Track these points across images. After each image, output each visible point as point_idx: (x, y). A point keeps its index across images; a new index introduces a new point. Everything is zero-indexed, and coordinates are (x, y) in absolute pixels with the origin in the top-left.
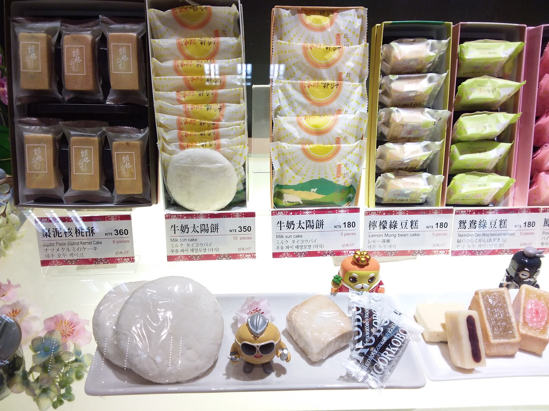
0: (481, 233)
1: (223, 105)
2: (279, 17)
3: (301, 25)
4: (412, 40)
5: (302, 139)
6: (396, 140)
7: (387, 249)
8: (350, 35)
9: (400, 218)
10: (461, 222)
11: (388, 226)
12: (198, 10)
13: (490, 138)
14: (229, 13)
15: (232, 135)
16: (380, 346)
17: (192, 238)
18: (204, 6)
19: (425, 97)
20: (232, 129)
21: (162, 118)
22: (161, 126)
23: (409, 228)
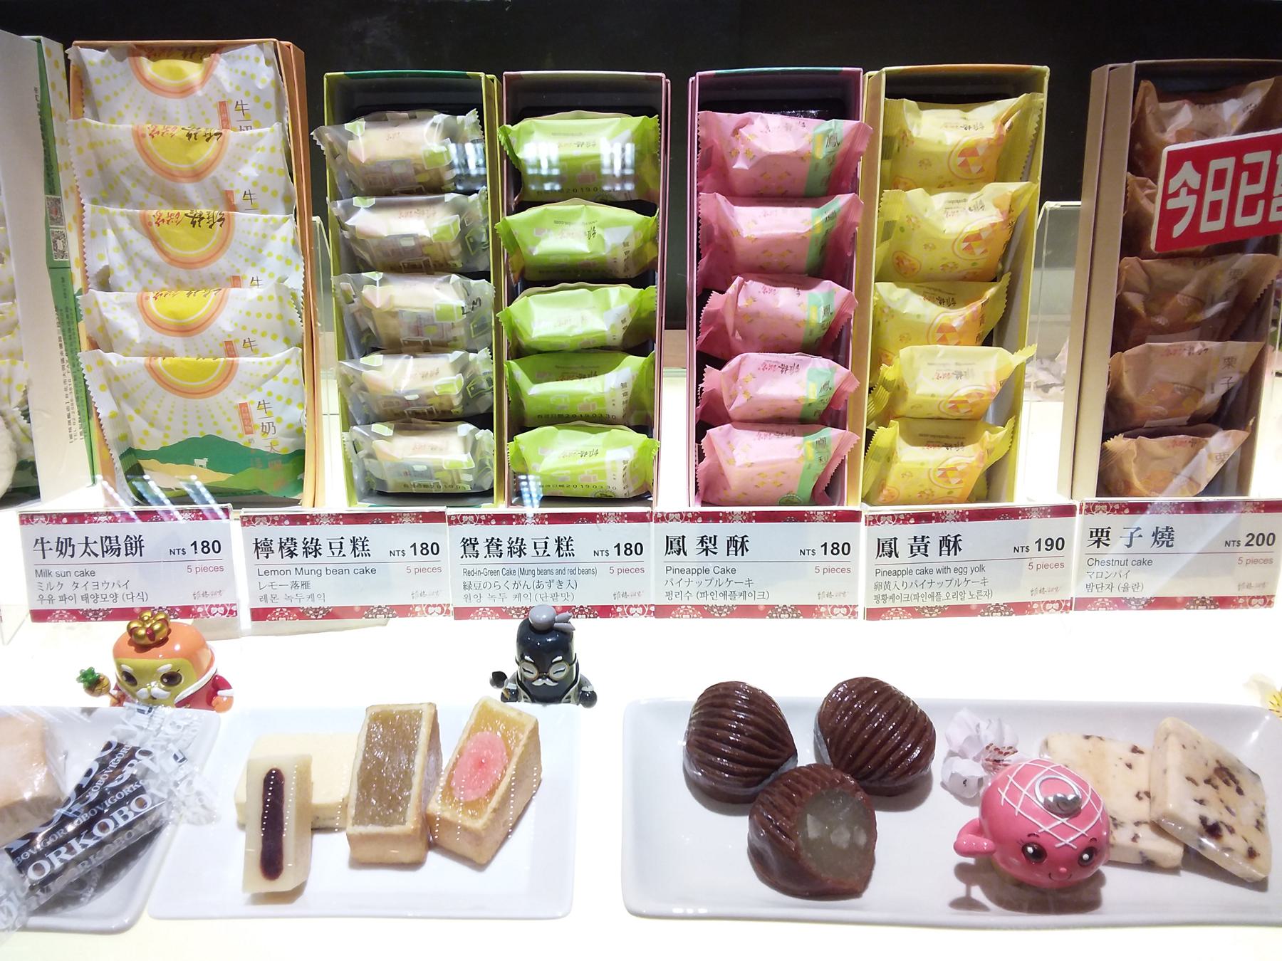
0: (516, 568)
4: (405, 114)
5: (147, 344)
6: (394, 347)
7: (305, 604)
8: (249, 104)
11: (300, 550)
17: (82, 568)
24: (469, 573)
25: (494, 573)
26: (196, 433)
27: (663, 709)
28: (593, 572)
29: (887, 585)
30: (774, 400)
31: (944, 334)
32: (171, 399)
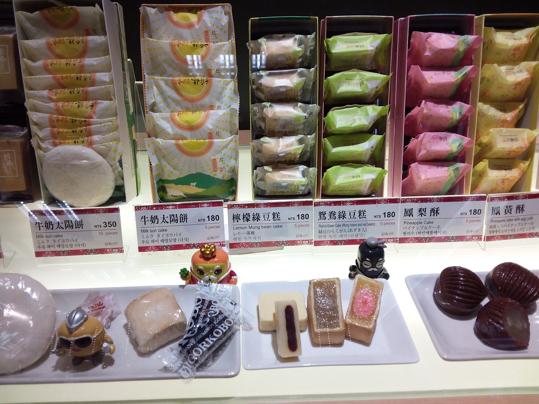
0: (341, 224)
1: (95, 103)
2: (146, 15)
3: (169, 22)
4: (281, 35)
5: (175, 134)
6: (273, 134)
7: (252, 241)
9: (348, 209)
10: (320, 213)
11: (251, 219)
12: (65, 10)
13: (364, 130)
14: (94, 13)
15: (105, 132)
16: (200, 337)
17: (161, 228)
18: (70, 7)
19: (297, 91)
20: (104, 125)
21: (35, 116)
22: (36, 124)
23: (272, 221)
24: (322, 226)
25: (332, 226)
26: (194, 172)
27: (425, 279)
28: (374, 224)
29: (495, 226)
30: (438, 152)
31: (503, 123)
32: (185, 157)
